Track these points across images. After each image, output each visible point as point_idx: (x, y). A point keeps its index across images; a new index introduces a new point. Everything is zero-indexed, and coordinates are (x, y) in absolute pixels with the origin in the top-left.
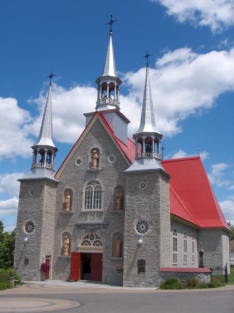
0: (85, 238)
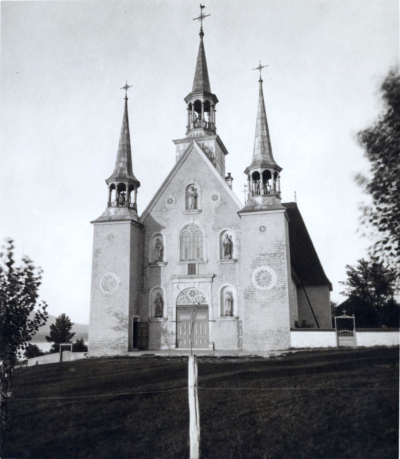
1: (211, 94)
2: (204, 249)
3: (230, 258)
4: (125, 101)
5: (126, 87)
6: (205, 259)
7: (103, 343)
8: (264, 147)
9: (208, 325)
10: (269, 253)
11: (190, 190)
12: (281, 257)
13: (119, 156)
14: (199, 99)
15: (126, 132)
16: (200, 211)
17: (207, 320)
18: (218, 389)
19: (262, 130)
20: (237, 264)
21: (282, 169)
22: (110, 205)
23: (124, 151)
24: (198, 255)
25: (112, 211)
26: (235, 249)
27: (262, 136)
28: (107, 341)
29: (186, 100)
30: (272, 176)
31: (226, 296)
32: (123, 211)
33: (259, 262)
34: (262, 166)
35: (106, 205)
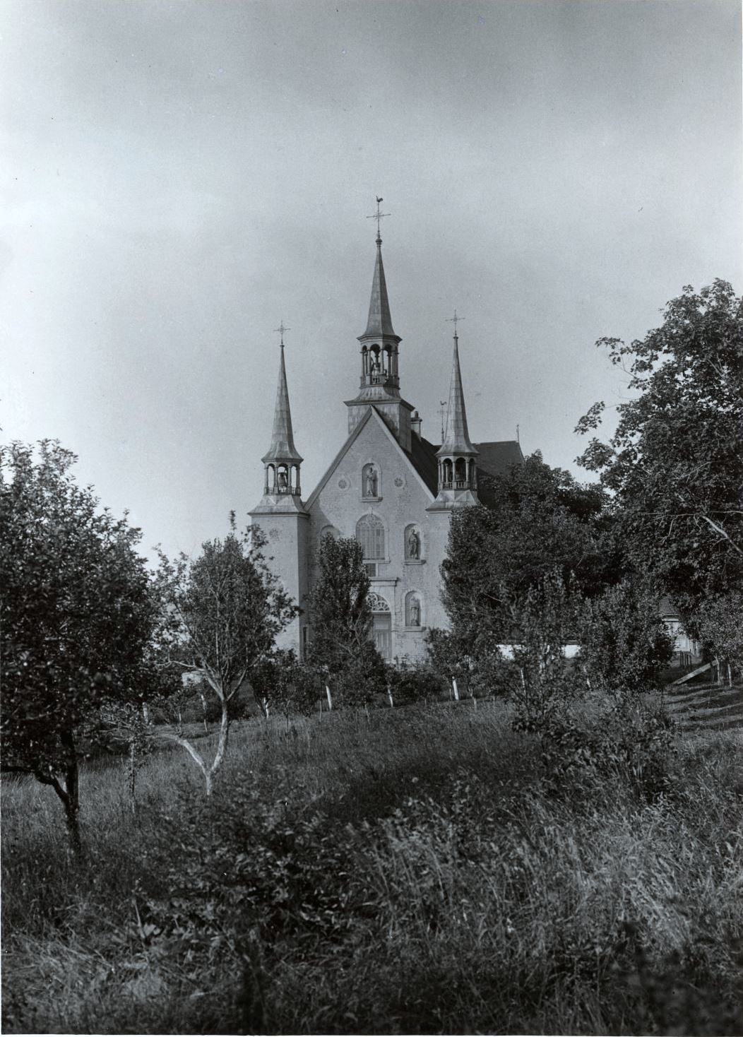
2: (386, 546)
3: (417, 558)
4: (280, 348)
5: (282, 330)
6: (387, 559)
8: (458, 427)
9: (390, 636)
11: (368, 472)
13: (279, 427)
14: (378, 343)
15: (284, 394)
16: (381, 499)
17: (389, 631)
18: (732, 679)
19: (457, 405)
20: (424, 566)
22: (267, 491)
23: (283, 419)
24: (378, 553)
25: (272, 499)
26: (422, 548)
27: (456, 413)
31: (412, 603)
32: (287, 503)
34: (455, 454)
35: (262, 491)
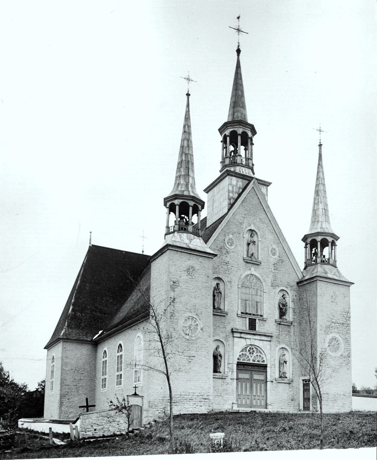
0: (242, 351)
1: (248, 123)
7: (184, 397)
10: (339, 321)
12: (347, 328)
21: (339, 238)
28: (189, 395)
29: (221, 130)
30: (330, 244)
33: (331, 329)
